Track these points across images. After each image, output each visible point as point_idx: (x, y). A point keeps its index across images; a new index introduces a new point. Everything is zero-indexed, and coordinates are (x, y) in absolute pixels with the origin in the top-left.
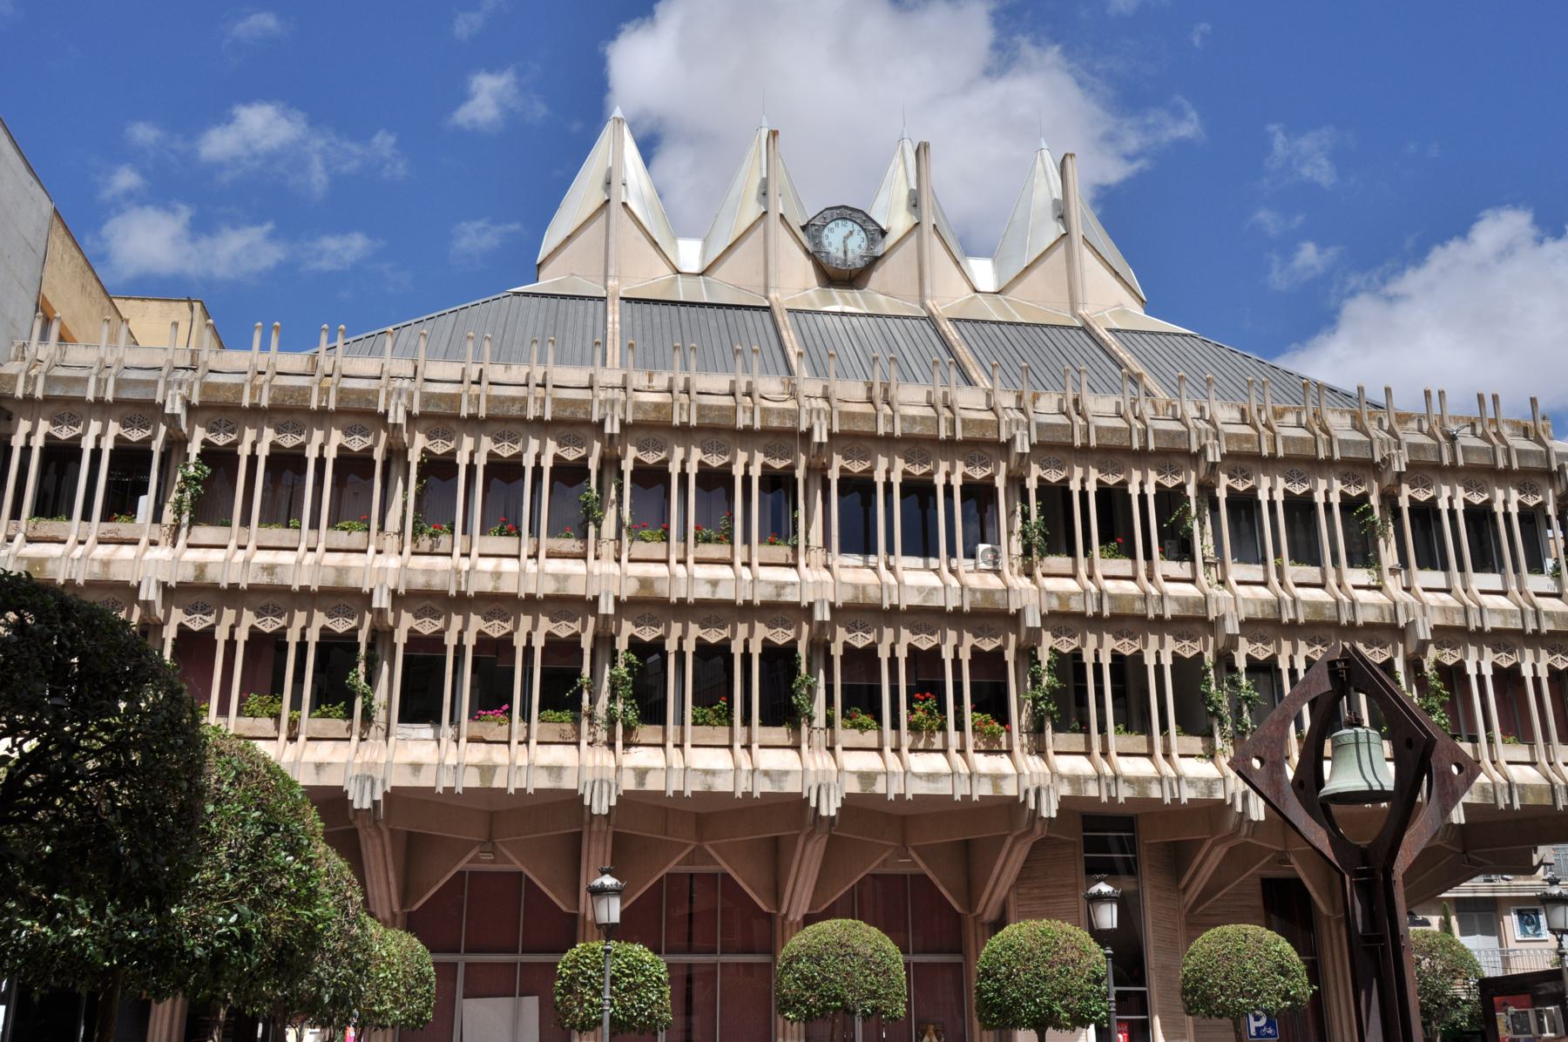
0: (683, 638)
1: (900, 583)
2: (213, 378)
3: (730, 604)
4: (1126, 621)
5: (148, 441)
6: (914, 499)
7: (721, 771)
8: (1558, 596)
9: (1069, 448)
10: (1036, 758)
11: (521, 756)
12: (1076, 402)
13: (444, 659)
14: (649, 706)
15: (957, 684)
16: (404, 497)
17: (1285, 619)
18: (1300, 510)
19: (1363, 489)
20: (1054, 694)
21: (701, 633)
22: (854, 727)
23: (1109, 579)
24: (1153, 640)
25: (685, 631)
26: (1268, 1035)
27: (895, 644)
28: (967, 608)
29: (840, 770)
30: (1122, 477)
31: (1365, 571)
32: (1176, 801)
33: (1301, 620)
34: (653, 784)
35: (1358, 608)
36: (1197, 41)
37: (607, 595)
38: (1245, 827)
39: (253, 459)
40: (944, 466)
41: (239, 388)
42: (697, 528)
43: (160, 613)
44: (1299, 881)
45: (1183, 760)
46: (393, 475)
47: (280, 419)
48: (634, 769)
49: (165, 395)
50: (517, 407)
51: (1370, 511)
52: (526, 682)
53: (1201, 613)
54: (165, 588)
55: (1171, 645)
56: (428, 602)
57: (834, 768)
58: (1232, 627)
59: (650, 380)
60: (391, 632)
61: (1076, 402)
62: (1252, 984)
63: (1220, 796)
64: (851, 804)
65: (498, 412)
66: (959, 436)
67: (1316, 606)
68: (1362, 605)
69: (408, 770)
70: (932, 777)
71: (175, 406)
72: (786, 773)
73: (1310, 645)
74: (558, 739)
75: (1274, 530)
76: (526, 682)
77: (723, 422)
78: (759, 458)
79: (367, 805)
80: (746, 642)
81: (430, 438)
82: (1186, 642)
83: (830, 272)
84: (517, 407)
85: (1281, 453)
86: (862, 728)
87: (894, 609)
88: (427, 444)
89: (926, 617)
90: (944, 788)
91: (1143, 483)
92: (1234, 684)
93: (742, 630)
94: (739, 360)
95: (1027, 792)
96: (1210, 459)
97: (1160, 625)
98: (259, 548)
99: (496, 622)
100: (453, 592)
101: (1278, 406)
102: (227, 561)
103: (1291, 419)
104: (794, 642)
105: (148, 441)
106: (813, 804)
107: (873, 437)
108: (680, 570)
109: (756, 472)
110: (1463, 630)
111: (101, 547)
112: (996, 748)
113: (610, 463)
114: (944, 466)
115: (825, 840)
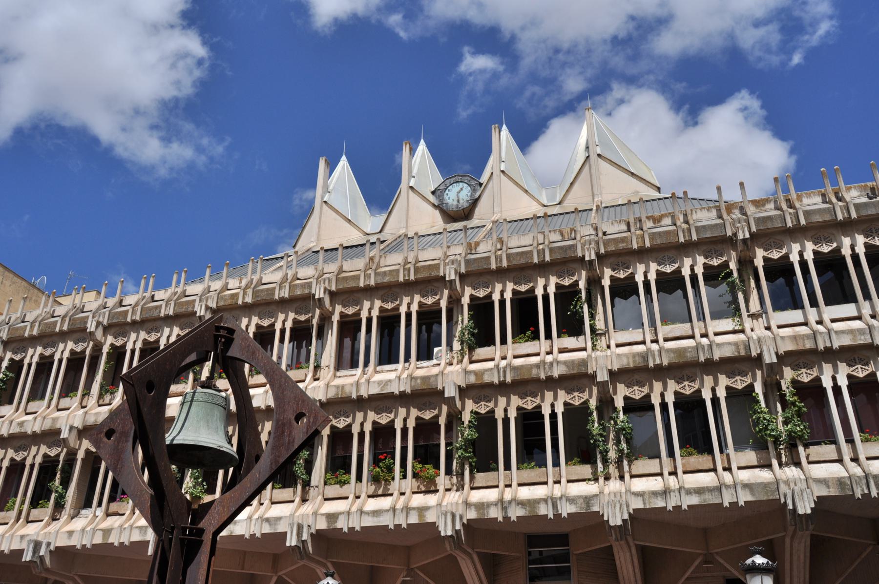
4: (684, 368)
10: (793, 468)
15: (404, 446)
17: (651, 364)
19: (724, 259)
20: (471, 444)
23: (505, 357)
24: (549, 395)
28: (408, 391)
32: (557, 516)
36: (230, 73)
40: (498, 287)
46: (746, 278)
49: (445, 269)
50: (157, 311)
51: (730, 274)
52: (555, 437)
54: (611, 373)
57: (803, 477)
63: (596, 509)
64: (637, 518)
68: (836, 332)
70: (699, 491)
71: (451, 275)
72: (280, 518)
73: (678, 383)
78: (510, 286)
82: (576, 394)
84: (157, 311)
86: (342, 483)
87: (360, 399)
89: (383, 401)
90: (711, 499)
91: (545, 287)
97: (552, 383)
103: (667, 221)
108: (655, 347)
110: (814, 352)
112: (433, 488)
113: (594, 283)
114: (541, 282)
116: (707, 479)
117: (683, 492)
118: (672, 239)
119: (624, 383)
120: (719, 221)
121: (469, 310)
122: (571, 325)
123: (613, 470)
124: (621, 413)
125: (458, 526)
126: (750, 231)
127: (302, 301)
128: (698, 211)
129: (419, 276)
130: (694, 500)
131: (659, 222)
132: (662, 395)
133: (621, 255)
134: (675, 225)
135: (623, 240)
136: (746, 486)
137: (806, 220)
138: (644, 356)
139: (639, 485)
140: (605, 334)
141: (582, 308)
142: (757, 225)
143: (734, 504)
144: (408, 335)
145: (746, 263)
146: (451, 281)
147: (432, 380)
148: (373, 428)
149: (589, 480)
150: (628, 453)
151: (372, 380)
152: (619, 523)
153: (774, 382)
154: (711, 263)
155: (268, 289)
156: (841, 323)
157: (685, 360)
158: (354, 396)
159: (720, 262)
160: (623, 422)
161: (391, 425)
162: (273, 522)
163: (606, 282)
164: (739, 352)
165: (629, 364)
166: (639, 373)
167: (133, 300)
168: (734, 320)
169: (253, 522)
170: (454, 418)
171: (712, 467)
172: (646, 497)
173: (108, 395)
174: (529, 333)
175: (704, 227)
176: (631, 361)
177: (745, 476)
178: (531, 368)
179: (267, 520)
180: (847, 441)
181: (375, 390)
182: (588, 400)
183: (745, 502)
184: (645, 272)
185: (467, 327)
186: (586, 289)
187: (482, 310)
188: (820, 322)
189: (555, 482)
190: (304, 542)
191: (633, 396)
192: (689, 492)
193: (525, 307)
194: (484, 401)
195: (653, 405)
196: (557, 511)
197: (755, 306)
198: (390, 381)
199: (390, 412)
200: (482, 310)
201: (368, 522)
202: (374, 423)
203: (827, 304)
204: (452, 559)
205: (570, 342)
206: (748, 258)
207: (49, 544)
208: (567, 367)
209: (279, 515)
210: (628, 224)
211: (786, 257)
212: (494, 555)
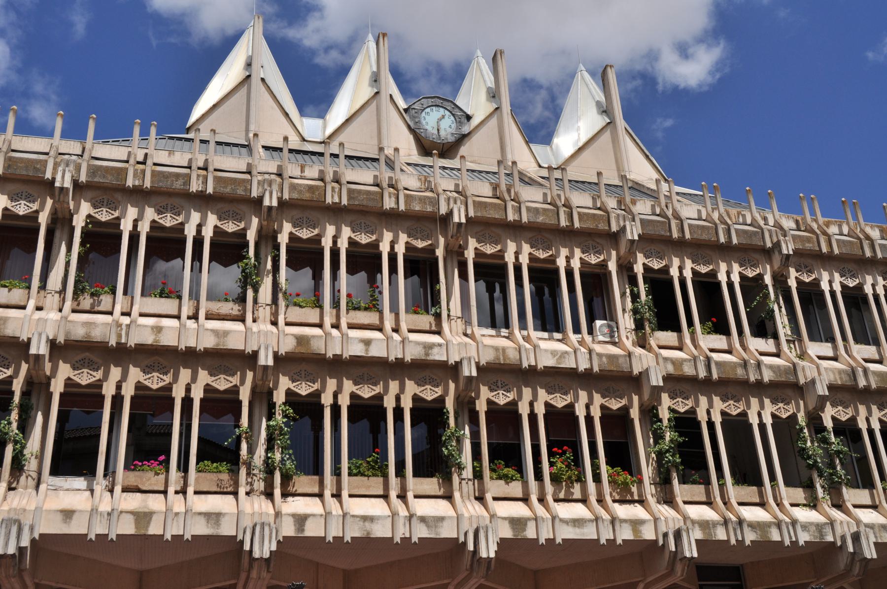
21: (354, 389)
27: (534, 402)
29: (493, 516)
34: (313, 530)
46: (262, 255)
47: (296, 213)
48: (294, 515)
53: (792, 379)
54: (53, 344)
56: (87, 354)
59: (302, 171)
69: (59, 517)
74: (215, 489)
87: (533, 370)
88: (92, 212)
91: (569, 260)
93: (394, 386)
112: (629, 497)
126: (467, 215)
133: (308, 207)
134: (190, 168)
137: (406, 205)
145: (267, 238)
146: (62, 189)
153: (266, 390)
158: (113, 342)
163: (79, 222)
165: (836, 380)
166: (302, 361)
167: (838, 234)
173: (87, 296)
176: (838, 377)
178: (736, 367)
183: (352, 538)
184: (337, 237)
194: (158, 371)
207: (32, 528)
208: (774, 372)
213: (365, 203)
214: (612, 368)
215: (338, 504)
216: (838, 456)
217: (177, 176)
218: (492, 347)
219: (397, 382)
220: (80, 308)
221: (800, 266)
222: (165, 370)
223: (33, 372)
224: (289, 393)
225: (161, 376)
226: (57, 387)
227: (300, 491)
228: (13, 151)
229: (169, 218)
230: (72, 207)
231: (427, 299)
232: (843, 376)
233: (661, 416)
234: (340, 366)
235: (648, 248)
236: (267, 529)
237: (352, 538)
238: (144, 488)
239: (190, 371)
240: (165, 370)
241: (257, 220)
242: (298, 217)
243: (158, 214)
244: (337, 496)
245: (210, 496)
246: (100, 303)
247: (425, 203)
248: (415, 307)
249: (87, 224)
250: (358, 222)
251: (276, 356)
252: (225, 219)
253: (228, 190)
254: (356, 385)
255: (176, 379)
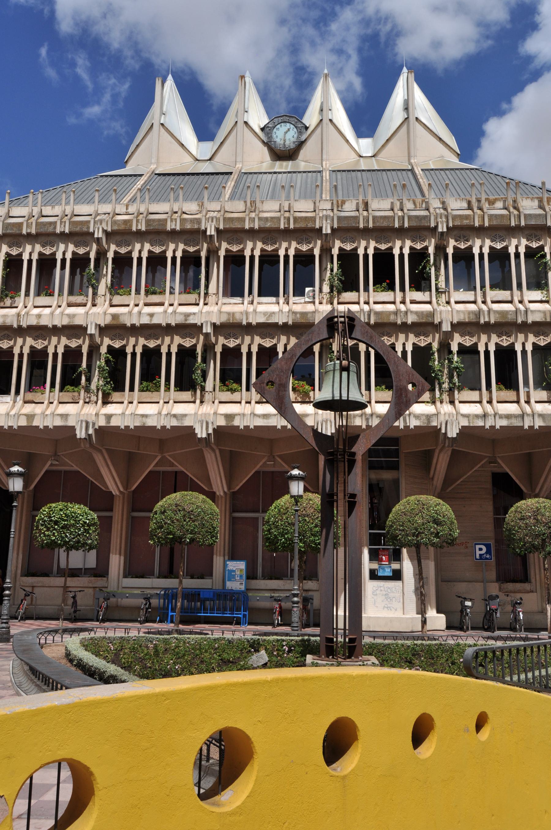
0: (135, 345)
1: (255, 311)
2: (185, 216)
3: (159, 326)
4: (505, 326)
5: (88, 253)
6: (497, 263)
7: (150, 415)
8: (547, 302)
9: (357, 230)
11: (248, 409)
12: (515, 201)
13: (12, 362)
14: (116, 381)
16: (218, 273)
17: (482, 321)
18: (500, 258)
19: (541, 243)
21: (145, 342)
22: (228, 390)
24: (402, 337)
25: (137, 342)
26: (487, 559)
27: (250, 344)
28: (290, 323)
29: (458, 413)
30: (390, 245)
31: (540, 292)
32: (407, 427)
33: (492, 321)
34: (114, 422)
35: (529, 313)
37: (91, 324)
38: (447, 441)
39: (140, 259)
40: (172, 246)
41: (20, 225)
42: (146, 286)
43: (98, 340)
44: (507, 474)
45: (462, 404)
47: (119, 238)
48: (105, 415)
50: (52, 227)
51: (544, 256)
52: (168, 369)
53: (430, 320)
54: (214, 325)
55: (412, 339)
56: (6, 332)
57: (454, 412)
58: (446, 327)
59: (127, 209)
60: (214, 346)
61: (515, 201)
62: (416, 529)
63: (434, 424)
64: (465, 432)
65: (42, 230)
66: (292, 226)
67: (503, 313)
68: (532, 311)
70: (508, 417)
72: (185, 415)
73: (499, 336)
74: (71, 401)
75: (483, 271)
76: (168, 369)
77: (160, 228)
78: (181, 246)
79: (204, 435)
80: (249, 346)
81: (10, 247)
82: (422, 338)
83: (278, 152)
84: (52, 227)
85: (487, 224)
86: (233, 391)
87: (249, 325)
88: (8, 250)
89: (268, 329)
90: (517, 423)
91: (401, 248)
92: (450, 361)
93: (248, 339)
94: (361, 190)
95: (318, 424)
96: (440, 230)
98: (180, 305)
99: (40, 341)
100: (15, 326)
101: (491, 197)
102: (130, 313)
103: (499, 204)
104: (195, 346)
105: (198, 251)
106: (443, 431)
107: (243, 231)
109: (486, 251)
111: (146, 308)
112: (307, 400)
114: (363, 243)
115: (449, 453)
116: (513, 408)
117: (497, 417)
118: (506, 222)
119: (459, 333)
120: (541, 212)
121: (338, 260)
122: (420, 281)
123: (445, 397)
124: (456, 355)
125: (91, 431)
127: (193, 234)
128: (524, 199)
129: (297, 226)
130: (504, 423)
131: (493, 204)
132: (486, 345)
135: (467, 217)
136: (541, 416)
138: (478, 314)
139: (465, 409)
140: (445, 292)
141: (430, 269)
142: (490, 220)
143: (531, 428)
144: (286, 275)
145: (441, 249)
146: (211, 236)
147: (309, 315)
148: (31, 351)
149: (428, 402)
150: (459, 386)
151: (90, 312)
152: (204, 435)
154: (531, 245)
155: (159, 220)
156: (533, 304)
157: (506, 320)
159: (538, 245)
160: (457, 362)
161: (238, 349)
162: (179, 418)
164: (546, 319)
165: (465, 319)
166: (115, 329)
168: (542, 293)
169: (163, 417)
170: (94, 349)
171: (516, 400)
172: (471, 418)
173: (8, 298)
174: (384, 284)
175: (530, 215)
177: (539, 408)
178: (390, 314)
179: (175, 416)
180: (487, 389)
181: (33, 322)
182: (430, 344)
184: (481, 246)
185: (337, 274)
186: (434, 254)
187: (348, 260)
188: (521, 302)
189: (247, 402)
190: (90, 436)
191: (465, 344)
192: (501, 417)
193: (384, 261)
194: (41, 339)
195: (479, 352)
196: (406, 424)
197: (442, 284)
198: (274, 313)
199: (273, 338)
200: (348, 260)
201: (260, 422)
202: (66, 347)
203: (529, 288)
204: (201, 452)
205: (418, 296)
206: (328, 247)
207: (94, 424)
208: (418, 316)
209: (184, 413)
210: (469, 203)
211: (506, 248)
212: (529, 453)
213: (157, 227)
214: (303, 321)
215: (491, 408)
216: (456, 371)
217: (385, 217)
218: (226, 312)
219: (57, 338)
220: (5, 306)
221: (460, 237)
222: (509, 335)
223: (207, 342)
224: (109, 347)
225: (43, 341)
226: (218, 349)
227: (114, 401)
228: (76, 215)
229: (48, 249)
230: (217, 246)
231: (191, 284)
232: (471, 315)
233: (333, 350)
234: (136, 330)
235: (345, 236)
236: (329, 422)
237: (500, 427)
238: (36, 401)
239: (404, 335)
240: (157, 337)
241: (320, 241)
242: (120, 240)
243: (43, 247)
244: (490, 402)
245: (68, 404)
246: (15, 302)
247: (194, 223)
248: (186, 290)
249: (6, 258)
250: (155, 239)
251: (452, 324)
252: (79, 246)
253: (78, 229)
254: (146, 340)
255: (279, 341)
